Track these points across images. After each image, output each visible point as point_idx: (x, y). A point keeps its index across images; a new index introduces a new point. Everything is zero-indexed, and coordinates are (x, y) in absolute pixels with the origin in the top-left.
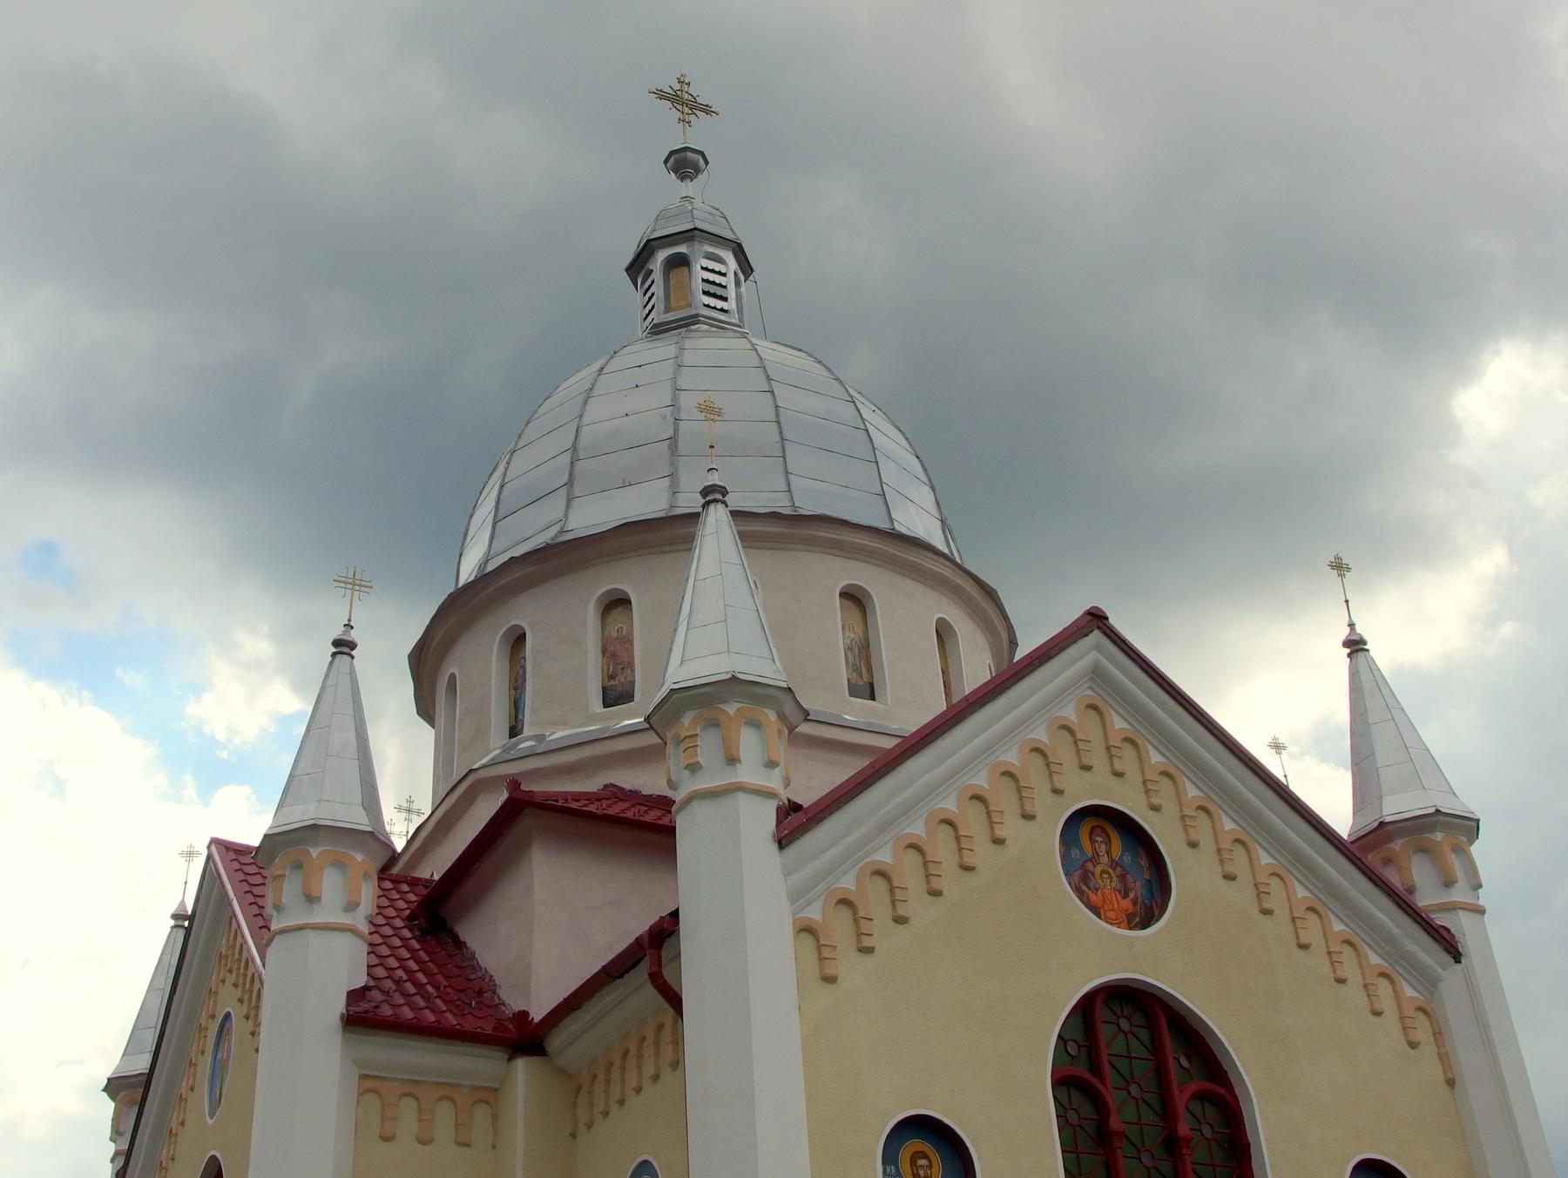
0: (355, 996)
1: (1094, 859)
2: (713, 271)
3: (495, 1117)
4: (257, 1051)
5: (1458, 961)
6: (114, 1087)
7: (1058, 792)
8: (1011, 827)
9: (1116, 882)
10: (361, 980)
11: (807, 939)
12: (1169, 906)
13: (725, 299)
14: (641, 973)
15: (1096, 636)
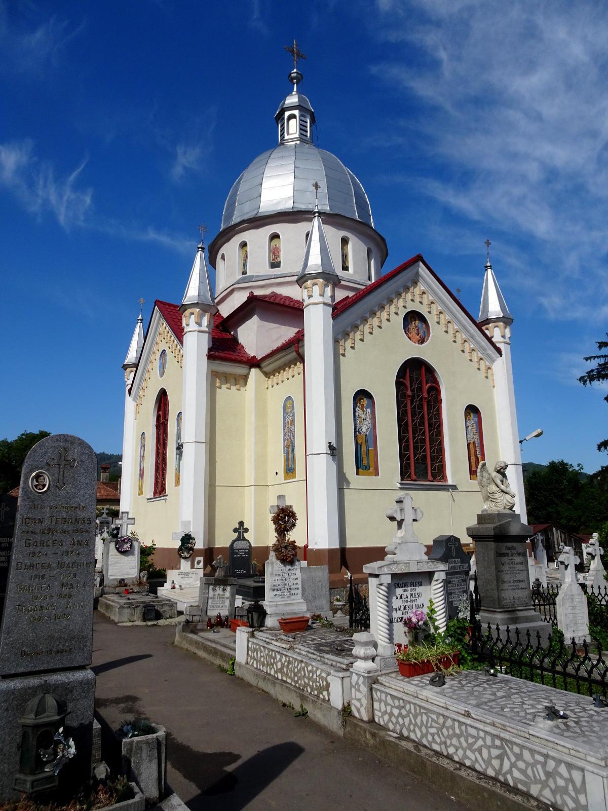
4: (494, 387)
5: (501, 356)
12: (427, 270)
14: (293, 348)
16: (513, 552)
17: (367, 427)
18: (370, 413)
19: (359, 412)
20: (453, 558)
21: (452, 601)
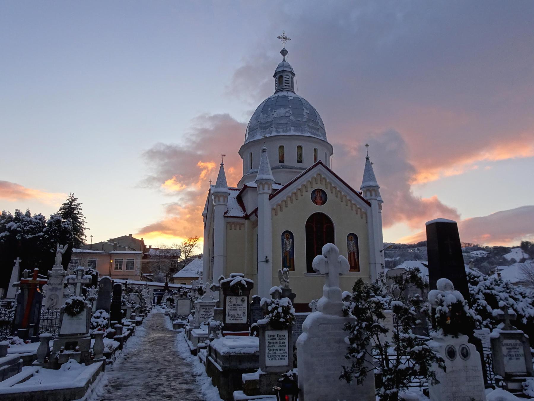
1: (317, 195)
2: (287, 78)
3: (244, 226)
7: (311, 187)
8: (304, 193)
9: (320, 199)
13: (289, 83)
15: (320, 165)
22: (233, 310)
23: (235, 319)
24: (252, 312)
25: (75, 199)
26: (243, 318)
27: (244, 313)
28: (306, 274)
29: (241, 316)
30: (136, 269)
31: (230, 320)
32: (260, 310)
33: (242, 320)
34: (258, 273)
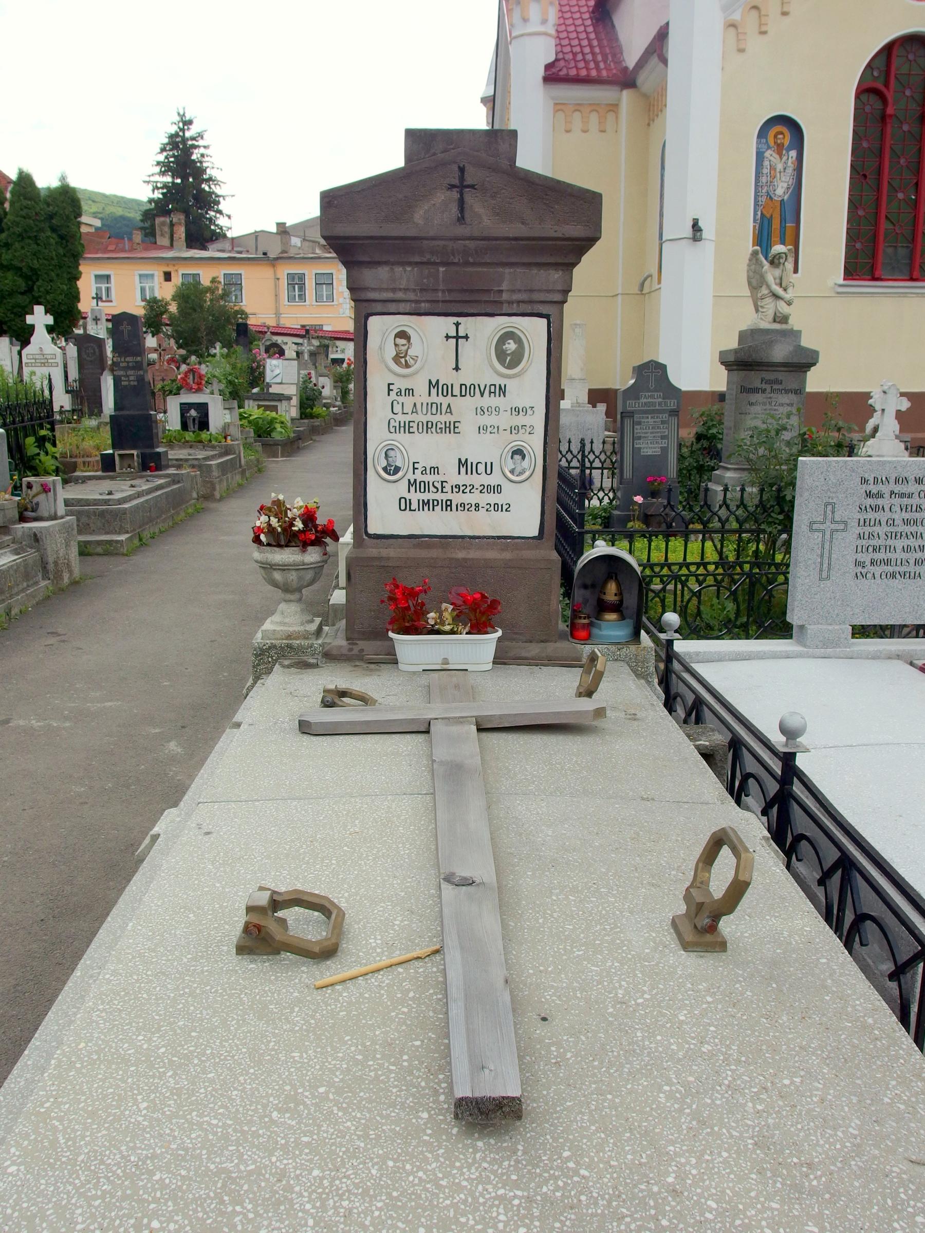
0: (548, 67)
3: (617, 118)
6: (484, 100)
10: (552, 58)
11: (732, 31)
16: (775, 387)
17: (785, 185)
18: (794, 158)
19: (772, 158)
20: (649, 391)
21: (639, 449)
22: (428, 427)
23: (448, 505)
24: (627, 422)
25: (190, 122)
26: (509, 493)
27: (519, 452)
28: (841, 286)
29: (494, 479)
30: (341, 300)
31: (405, 505)
32: (665, 416)
33: (497, 507)
34: (662, 285)
